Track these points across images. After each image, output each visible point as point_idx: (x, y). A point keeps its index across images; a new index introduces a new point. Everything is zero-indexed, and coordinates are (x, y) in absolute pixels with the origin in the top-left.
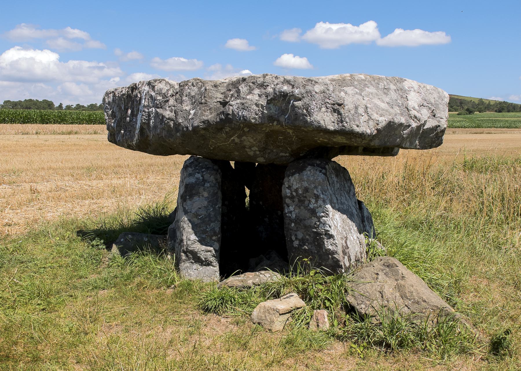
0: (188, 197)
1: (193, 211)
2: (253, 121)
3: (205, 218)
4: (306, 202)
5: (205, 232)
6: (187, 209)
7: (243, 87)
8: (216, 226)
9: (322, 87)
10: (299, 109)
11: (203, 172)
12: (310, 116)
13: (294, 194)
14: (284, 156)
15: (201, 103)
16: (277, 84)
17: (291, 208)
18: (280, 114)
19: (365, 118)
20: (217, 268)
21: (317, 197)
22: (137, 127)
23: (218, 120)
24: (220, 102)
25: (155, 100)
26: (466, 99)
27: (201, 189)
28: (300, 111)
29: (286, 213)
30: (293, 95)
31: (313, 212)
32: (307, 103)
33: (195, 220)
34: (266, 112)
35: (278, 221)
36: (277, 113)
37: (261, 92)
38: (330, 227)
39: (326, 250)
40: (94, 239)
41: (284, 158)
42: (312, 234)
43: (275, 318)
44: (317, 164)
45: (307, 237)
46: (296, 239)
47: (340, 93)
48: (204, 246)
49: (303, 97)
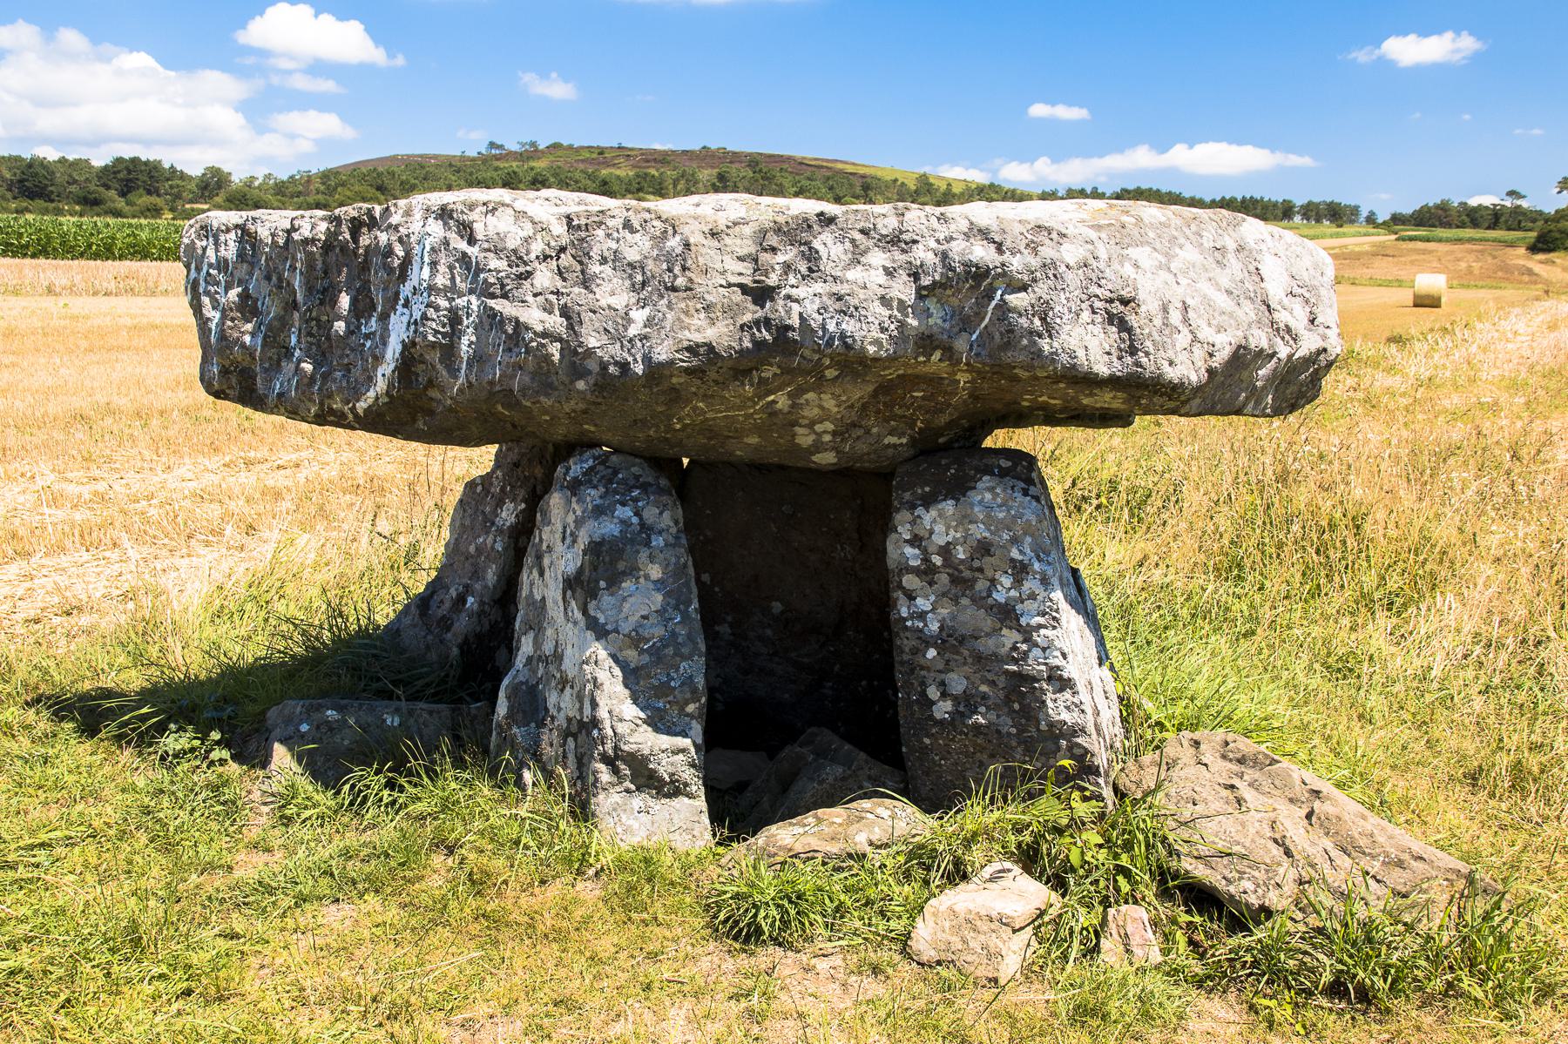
0: (602, 584)
1: (626, 627)
2: (871, 349)
3: (665, 646)
4: (981, 585)
5: (663, 690)
6: (602, 620)
7: (830, 242)
8: (694, 669)
9: (1081, 250)
10: (1021, 315)
11: (636, 500)
12: (1050, 336)
13: (937, 560)
14: (895, 446)
15: (674, 289)
16: (950, 239)
17: (923, 604)
18: (956, 329)
19: (1183, 339)
20: (701, 803)
21: (1020, 571)
22: (389, 355)
23: (747, 344)
24: (741, 286)
25: (479, 270)
26: (879, 174)
27: (643, 555)
28: (1023, 321)
29: (905, 620)
30: (1004, 274)
31: (1007, 614)
32: (1046, 297)
33: (631, 655)
34: (915, 323)
35: (769, 632)
36: (947, 325)
37: (894, 261)
38: (1064, 656)
39: (1051, 725)
40: (161, 729)
41: (890, 451)
42: (1003, 678)
43: (1000, 945)
44: (999, 466)
45: (984, 688)
46: (944, 695)
47: (1122, 264)
48: (665, 737)
49: (1035, 280)
